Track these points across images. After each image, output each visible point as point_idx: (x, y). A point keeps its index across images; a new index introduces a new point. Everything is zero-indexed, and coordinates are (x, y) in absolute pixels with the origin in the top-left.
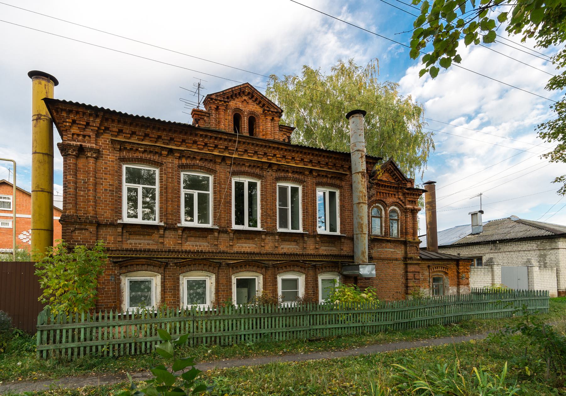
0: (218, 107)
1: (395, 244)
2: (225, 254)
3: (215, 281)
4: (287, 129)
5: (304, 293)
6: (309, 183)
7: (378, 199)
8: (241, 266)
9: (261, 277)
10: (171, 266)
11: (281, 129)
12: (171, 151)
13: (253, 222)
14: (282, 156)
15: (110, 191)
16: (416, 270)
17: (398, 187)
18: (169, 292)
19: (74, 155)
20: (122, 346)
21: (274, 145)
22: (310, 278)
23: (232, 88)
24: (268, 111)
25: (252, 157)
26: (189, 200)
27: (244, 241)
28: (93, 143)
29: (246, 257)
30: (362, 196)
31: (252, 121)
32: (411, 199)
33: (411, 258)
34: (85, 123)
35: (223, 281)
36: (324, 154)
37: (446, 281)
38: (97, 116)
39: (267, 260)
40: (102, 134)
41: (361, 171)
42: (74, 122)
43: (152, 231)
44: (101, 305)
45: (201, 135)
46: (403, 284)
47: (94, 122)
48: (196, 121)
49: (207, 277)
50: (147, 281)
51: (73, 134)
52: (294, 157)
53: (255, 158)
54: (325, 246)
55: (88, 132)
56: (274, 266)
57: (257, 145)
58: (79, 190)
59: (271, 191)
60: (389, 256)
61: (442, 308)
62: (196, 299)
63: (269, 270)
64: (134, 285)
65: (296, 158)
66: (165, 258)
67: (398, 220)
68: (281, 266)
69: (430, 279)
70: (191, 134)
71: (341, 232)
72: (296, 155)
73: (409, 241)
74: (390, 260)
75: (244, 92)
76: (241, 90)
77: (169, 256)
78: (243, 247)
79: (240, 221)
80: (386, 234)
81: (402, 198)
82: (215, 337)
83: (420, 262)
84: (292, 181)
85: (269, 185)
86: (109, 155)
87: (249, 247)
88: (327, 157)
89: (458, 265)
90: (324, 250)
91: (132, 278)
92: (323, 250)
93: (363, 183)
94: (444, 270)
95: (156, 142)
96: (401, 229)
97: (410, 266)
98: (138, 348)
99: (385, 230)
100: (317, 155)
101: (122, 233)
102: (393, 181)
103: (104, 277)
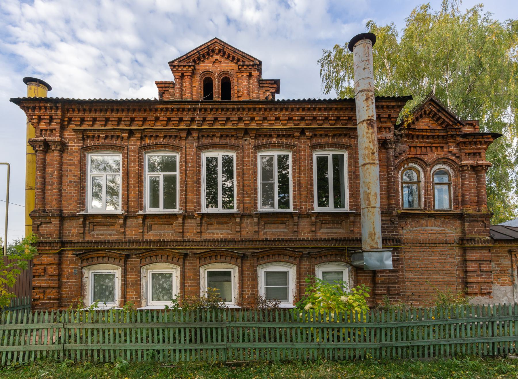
0: (182, 74)
1: (443, 219)
2: (191, 243)
3: (179, 275)
4: (269, 83)
6: (301, 147)
7: (410, 156)
9: (237, 269)
10: (133, 258)
11: (261, 85)
13: (338, 203)
14: (262, 119)
16: (483, 258)
17: (447, 135)
18: (131, 286)
19: (41, 150)
21: (249, 106)
22: (304, 271)
23: (197, 48)
27: (216, 226)
28: (58, 136)
30: (369, 154)
31: (226, 85)
32: (472, 151)
33: (472, 240)
39: (244, 248)
40: (68, 125)
41: (367, 118)
44: (65, 300)
45: (162, 109)
46: (460, 278)
47: (56, 114)
48: (161, 95)
49: (173, 270)
50: (112, 274)
51: (41, 130)
52: (279, 117)
56: (309, 255)
57: (228, 109)
58: (48, 185)
59: (249, 163)
60: (433, 238)
62: (161, 295)
63: (247, 261)
65: (281, 118)
66: (127, 249)
67: (449, 184)
68: (261, 256)
69: (513, 270)
71: (351, 208)
73: (468, 215)
74: (435, 244)
75: (213, 51)
76: (208, 49)
77: (130, 247)
78: (213, 234)
80: (428, 205)
81: (455, 151)
83: (490, 245)
84: (278, 147)
85: (246, 156)
86: (74, 146)
87: (222, 234)
88: (325, 109)
91: (154, 270)
92: (323, 233)
93: (369, 135)
96: (454, 197)
97: (472, 251)
99: (425, 201)
102: (439, 128)
103: (68, 271)
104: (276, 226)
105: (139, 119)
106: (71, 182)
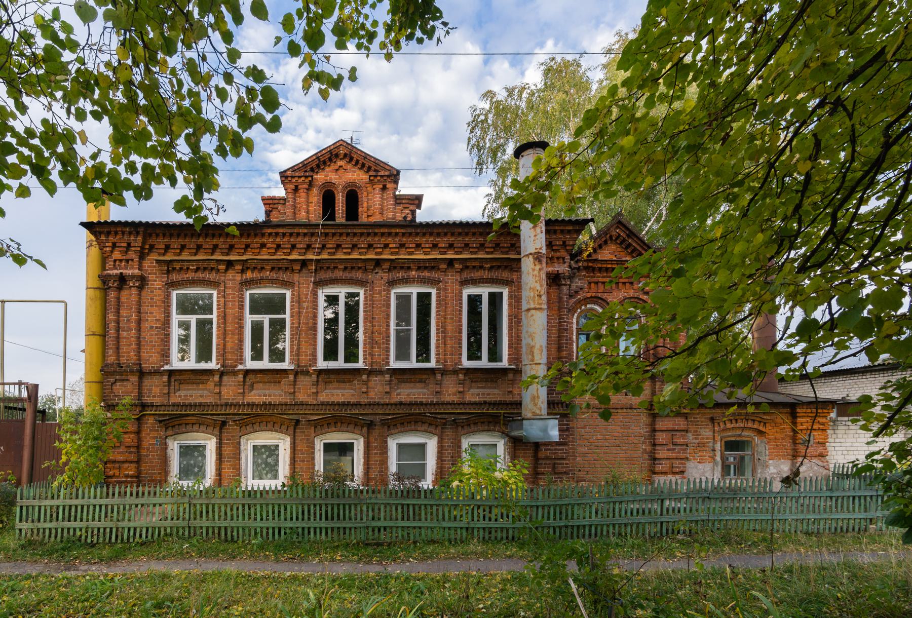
0: (297, 187)
5: (435, 467)
7: (589, 295)
8: (329, 424)
9: (362, 440)
12: (230, 264)
13: (351, 356)
15: (156, 327)
16: (676, 427)
20: (102, 530)
21: (382, 230)
24: (376, 176)
25: (349, 254)
26: (257, 329)
27: (336, 384)
29: (329, 412)
31: (352, 198)
34: (125, 245)
35: (447, 443)
36: (473, 230)
37: (761, 448)
38: (138, 233)
40: (148, 254)
41: (533, 251)
42: (114, 246)
43: (205, 377)
45: (270, 234)
46: (646, 453)
47: (135, 241)
48: (268, 213)
51: (115, 261)
53: (355, 256)
54: (478, 388)
55: (132, 255)
57: (355, 234)
61: (829, 503)
64: (186, 451)
70: (256, 235)
71: (510, 362)
72: (422, 240)
75: (337, 155)
78: (333, 395)
79: (474, 354)
82: (220, 528)
87: (343, 395)
89: (794, 416)
90: (474, 394)
94: (755, 426)
95: (212, 254)
98: (120, 534)
100: (460, 234)
101: (317, 381)
104: (412, 385)
105: (240, 246)
106: (152, 327)
